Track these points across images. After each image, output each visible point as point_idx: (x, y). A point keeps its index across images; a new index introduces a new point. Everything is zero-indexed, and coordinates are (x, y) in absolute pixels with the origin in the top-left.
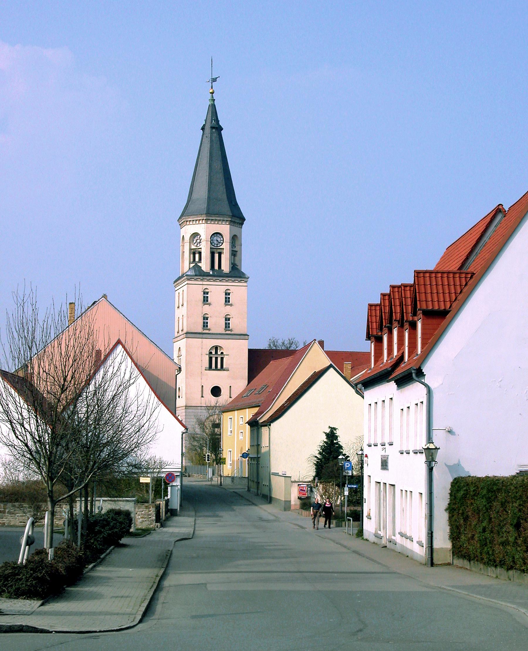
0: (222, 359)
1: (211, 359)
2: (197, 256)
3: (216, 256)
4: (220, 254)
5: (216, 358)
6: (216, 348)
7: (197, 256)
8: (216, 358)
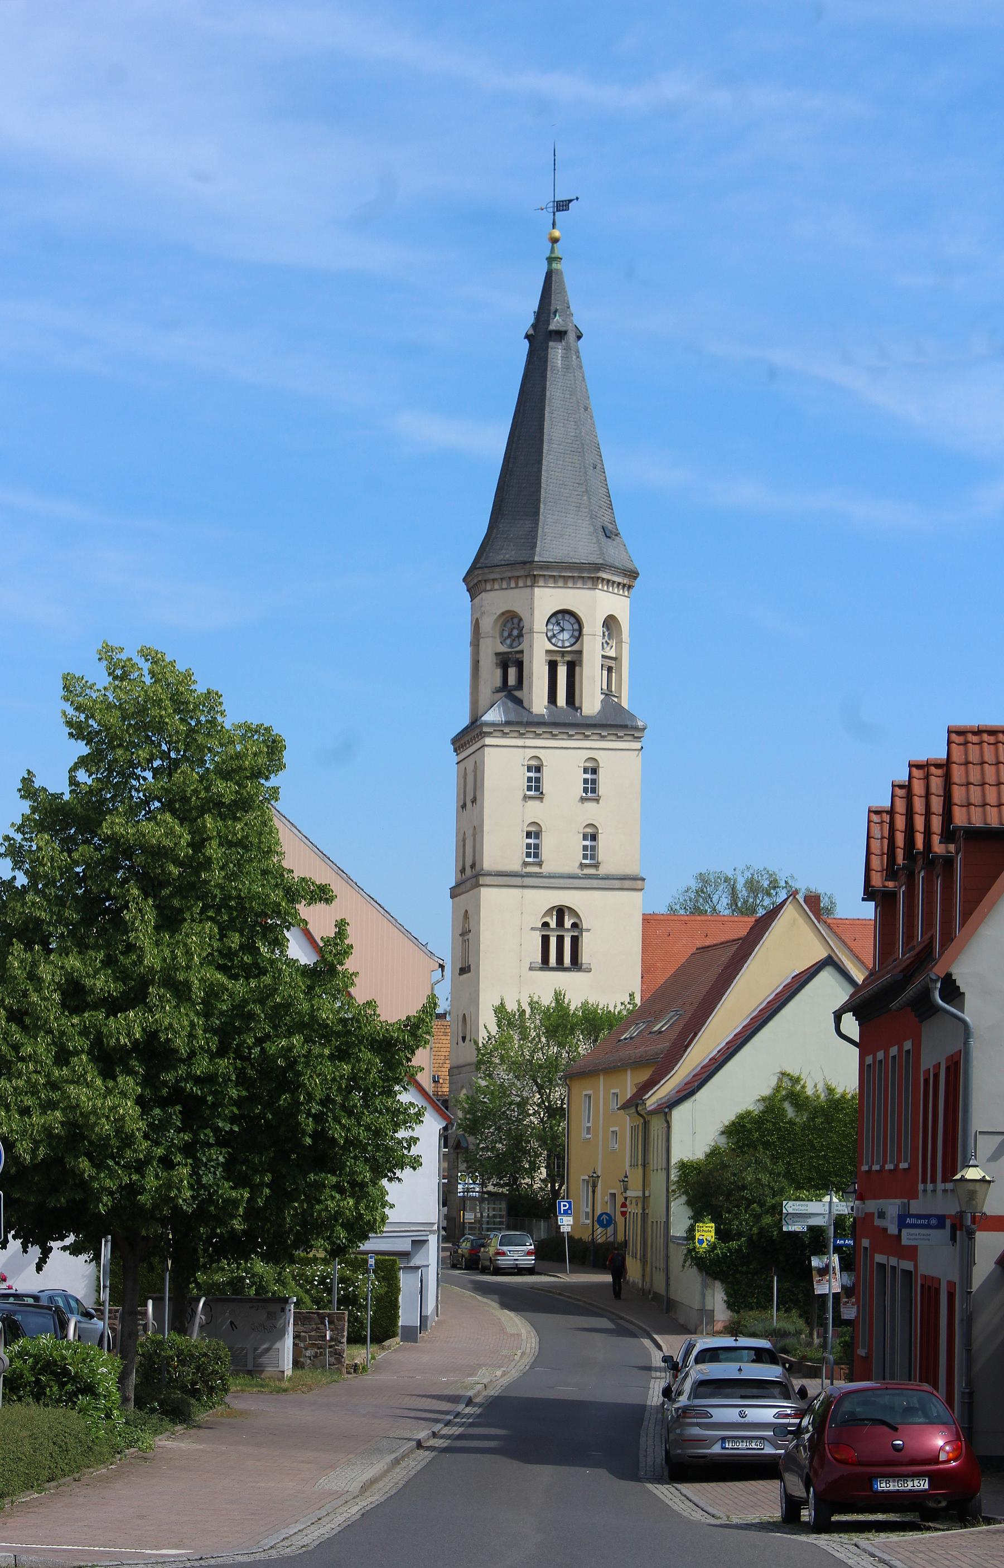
1: (545, 940)
2: (512, 672)
3: (562, 671)
4: (572, 668)
5: (560, 940)
6: (560, 912)
7: (512, 672)
8: (560, 940)
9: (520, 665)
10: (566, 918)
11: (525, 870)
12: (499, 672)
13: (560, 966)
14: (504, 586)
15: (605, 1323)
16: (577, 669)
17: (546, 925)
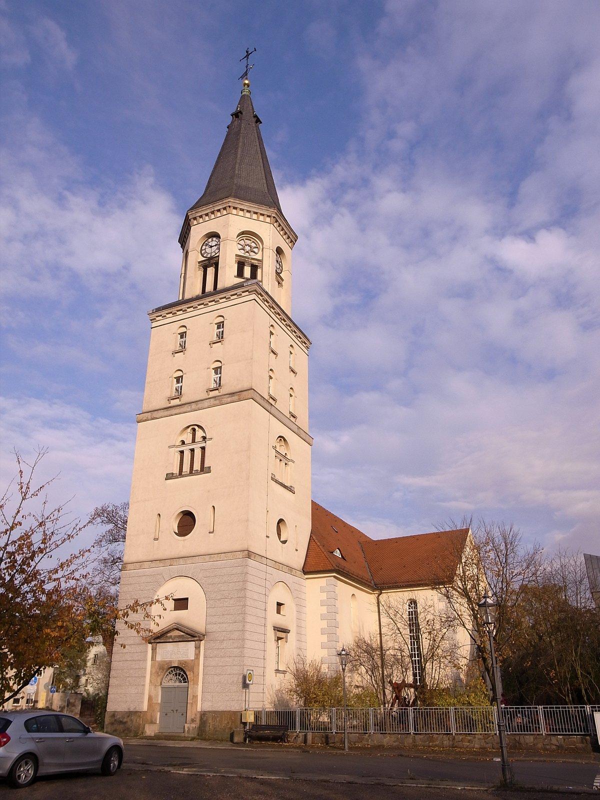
1: (182, 452)
6: (193, 429)
9: (216, 266)
13: (192, 472)
16: (259, 271)
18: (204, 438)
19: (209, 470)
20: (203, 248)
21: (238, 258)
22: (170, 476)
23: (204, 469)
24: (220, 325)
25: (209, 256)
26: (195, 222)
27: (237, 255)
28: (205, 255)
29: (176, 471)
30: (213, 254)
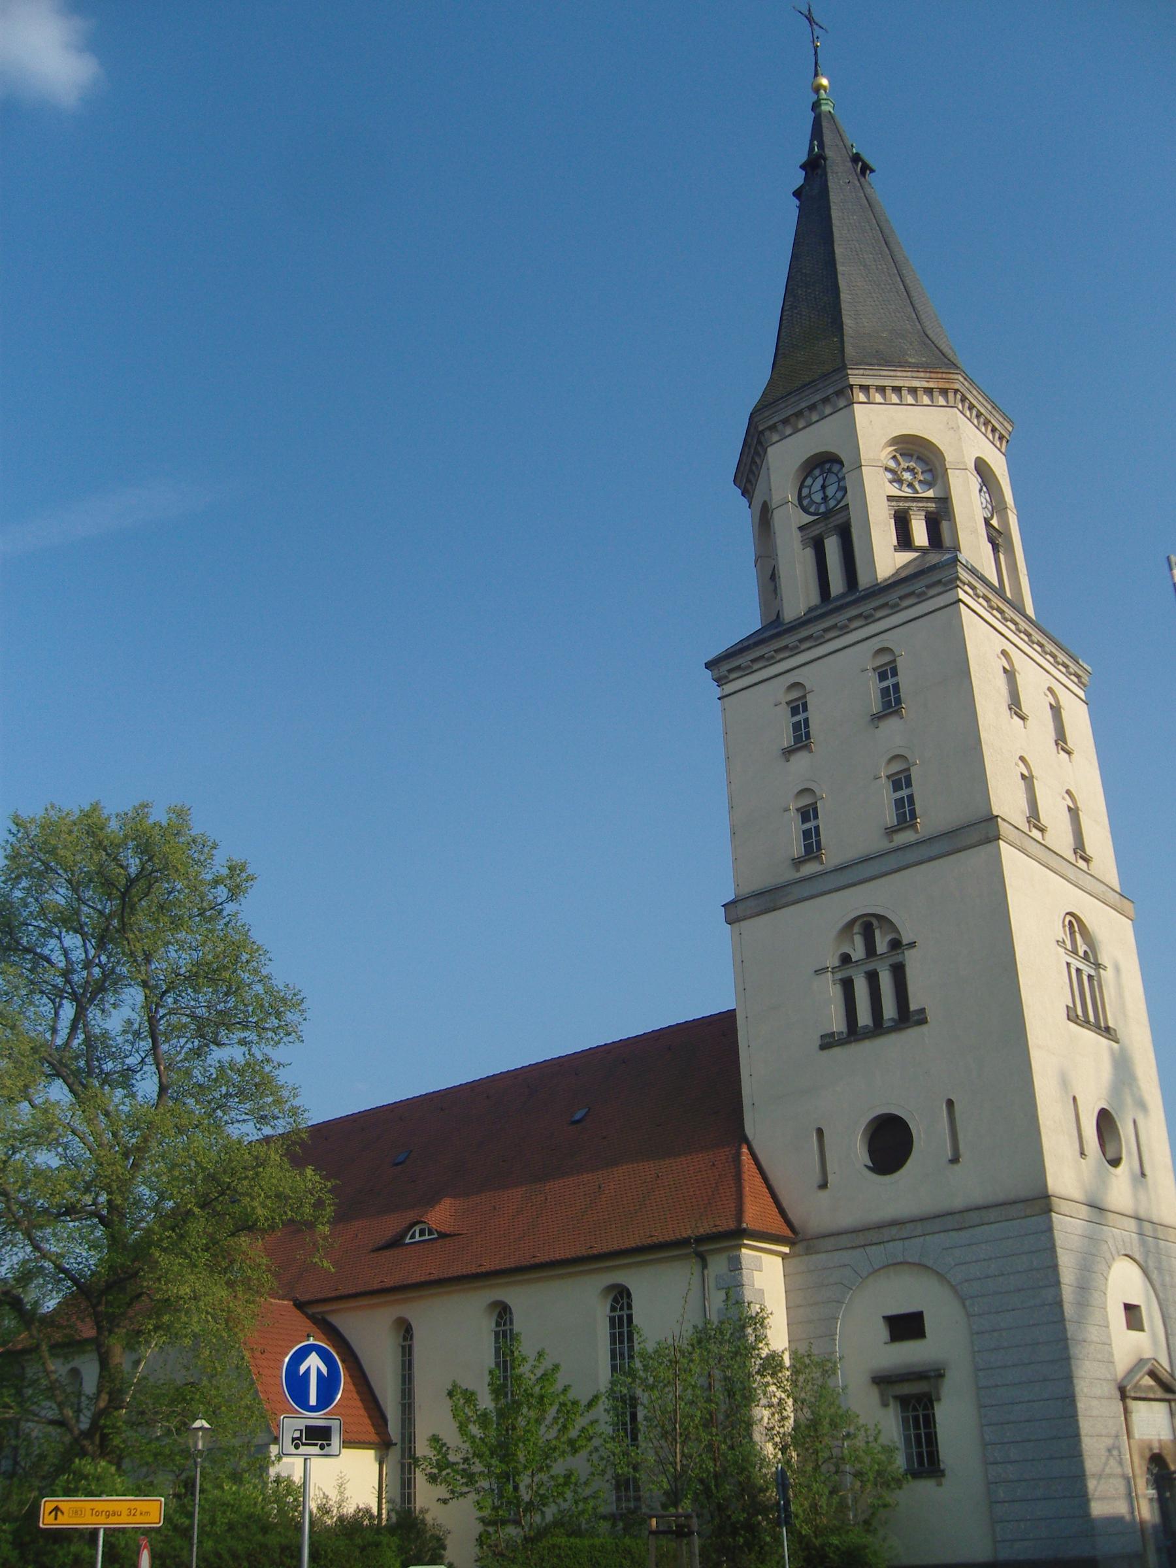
0: (899, 971)
1: (847, 986)
3: (832, 545)
5: (873, 978)
6: (868, 925)
8: (873, 978)
10: (877, 933)
11: (798, 875)
12: (809, 553)
13: (878, 1027)
14: (801, 425)
15: (1082, 694)
16: (945, 525)
17: (846, 959)
18: (896, 944)
19: (921, 1019)
20: (803, 495)
21: (894, 503)
22: (828, 1042)
23: (908, 1018)
24: (798, 707)
25: (822, 509)
26: (775, 438)
27: (890, 498)
28: (812, 510)
29: (837, 1023)
30: (832, 503)
